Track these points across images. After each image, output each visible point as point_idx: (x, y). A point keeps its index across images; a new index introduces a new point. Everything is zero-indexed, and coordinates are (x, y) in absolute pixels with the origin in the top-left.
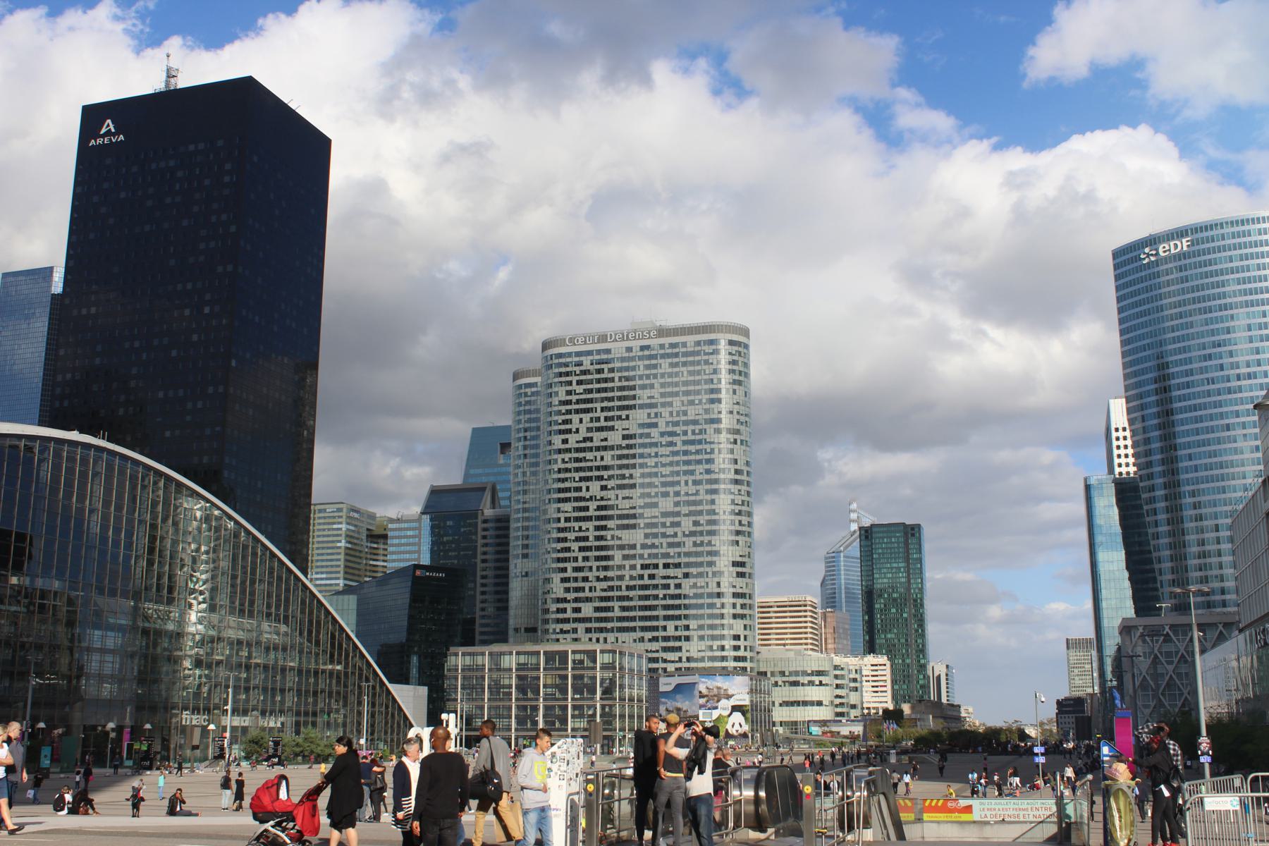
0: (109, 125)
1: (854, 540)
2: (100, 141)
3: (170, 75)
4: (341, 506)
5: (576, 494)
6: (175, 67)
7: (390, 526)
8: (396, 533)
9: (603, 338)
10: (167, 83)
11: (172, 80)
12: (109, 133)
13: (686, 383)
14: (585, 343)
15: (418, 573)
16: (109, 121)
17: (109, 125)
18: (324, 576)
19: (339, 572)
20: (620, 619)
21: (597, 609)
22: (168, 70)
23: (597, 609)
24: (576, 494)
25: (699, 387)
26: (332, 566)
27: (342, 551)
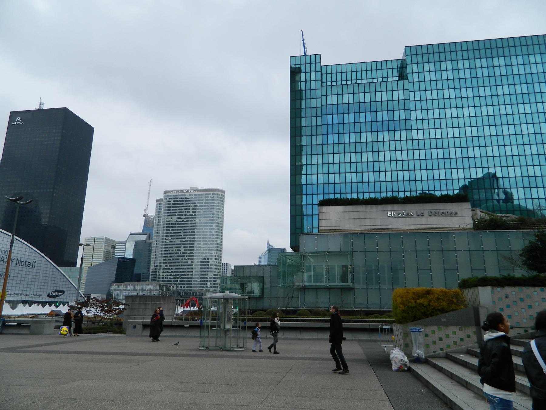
0: (19, 118)
1: (266, 254)
2: (15, 123)
3: (41, 104)
4: (103, 238)
5: (191, 222)
6: (43, 102)
7: (117, 245)
8: (86, 258)
9: (181, 191)
10: (40, 107)
11: (42, 106)
12: (18, 121)
13: (203, 232)
14: (176, 192)
15: (120, 259)
16: (19, 117)
17: (19, 118)
18: (96, 259)
19: (101, 258)
20: (205, 206)
21: (204, 212)
22: (41, 102)
23: (204, 212)
24: (191, 222)
25: (199, 255)
26: (99, 256)
27: (103, 252)
